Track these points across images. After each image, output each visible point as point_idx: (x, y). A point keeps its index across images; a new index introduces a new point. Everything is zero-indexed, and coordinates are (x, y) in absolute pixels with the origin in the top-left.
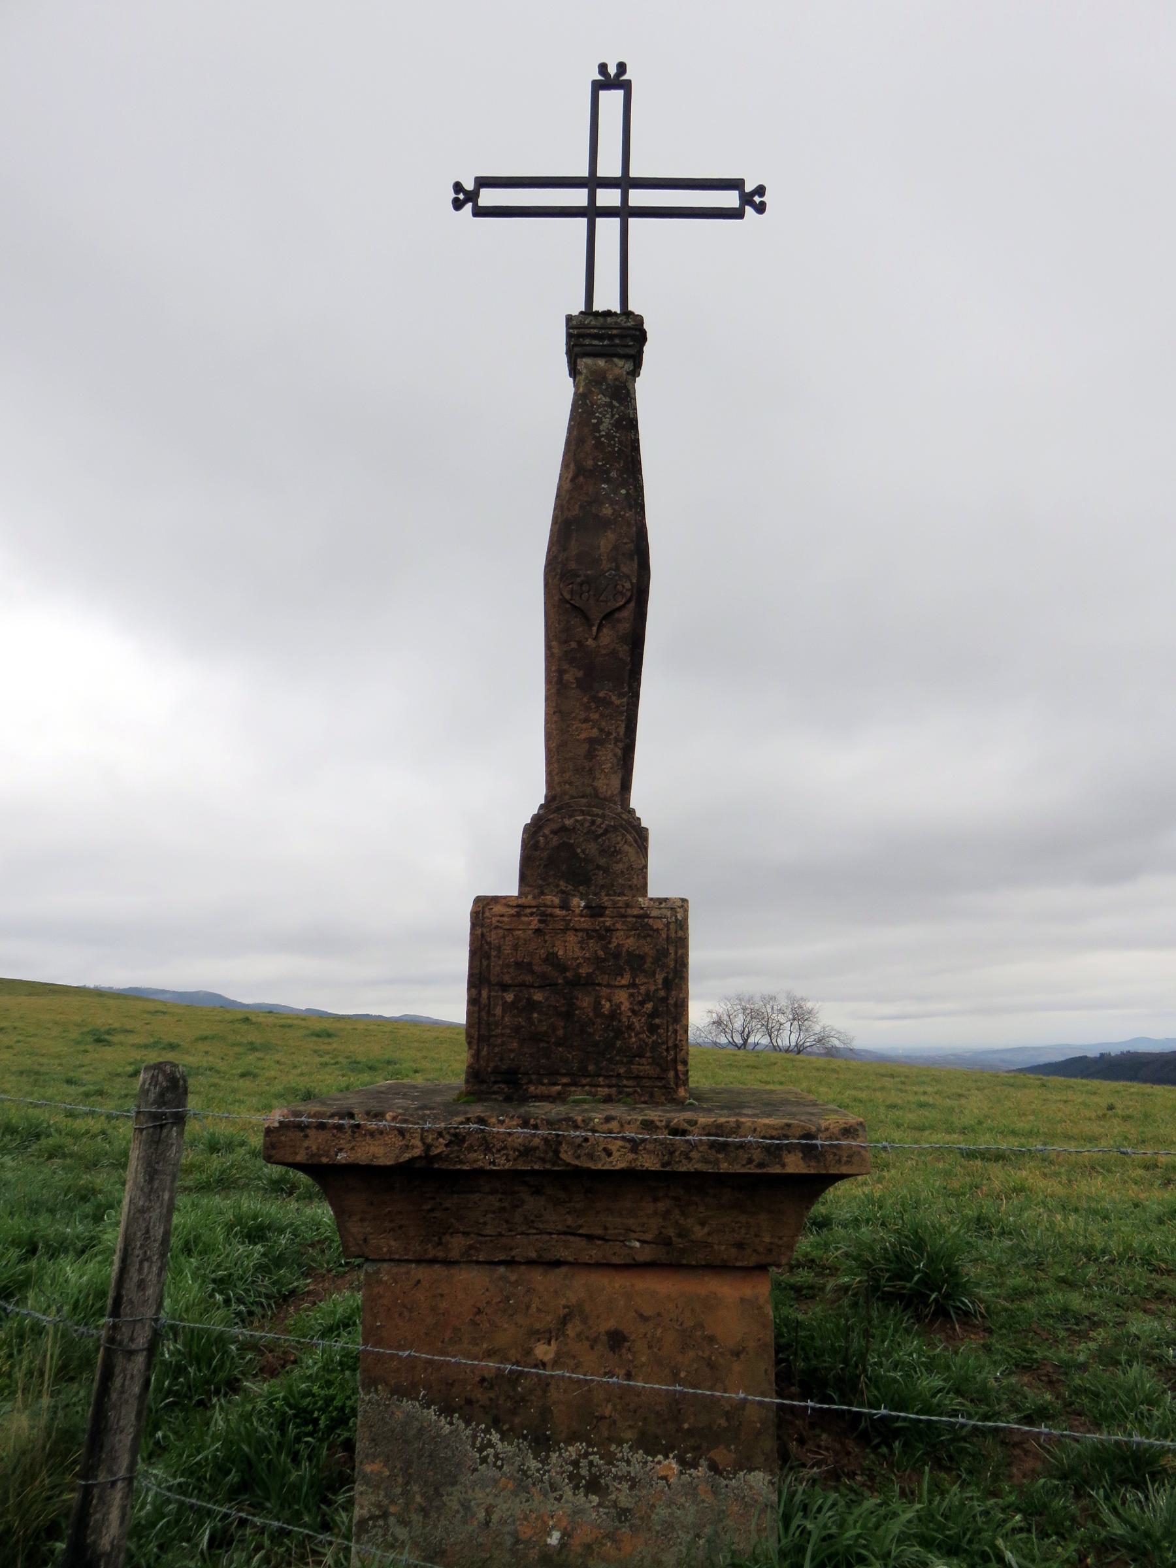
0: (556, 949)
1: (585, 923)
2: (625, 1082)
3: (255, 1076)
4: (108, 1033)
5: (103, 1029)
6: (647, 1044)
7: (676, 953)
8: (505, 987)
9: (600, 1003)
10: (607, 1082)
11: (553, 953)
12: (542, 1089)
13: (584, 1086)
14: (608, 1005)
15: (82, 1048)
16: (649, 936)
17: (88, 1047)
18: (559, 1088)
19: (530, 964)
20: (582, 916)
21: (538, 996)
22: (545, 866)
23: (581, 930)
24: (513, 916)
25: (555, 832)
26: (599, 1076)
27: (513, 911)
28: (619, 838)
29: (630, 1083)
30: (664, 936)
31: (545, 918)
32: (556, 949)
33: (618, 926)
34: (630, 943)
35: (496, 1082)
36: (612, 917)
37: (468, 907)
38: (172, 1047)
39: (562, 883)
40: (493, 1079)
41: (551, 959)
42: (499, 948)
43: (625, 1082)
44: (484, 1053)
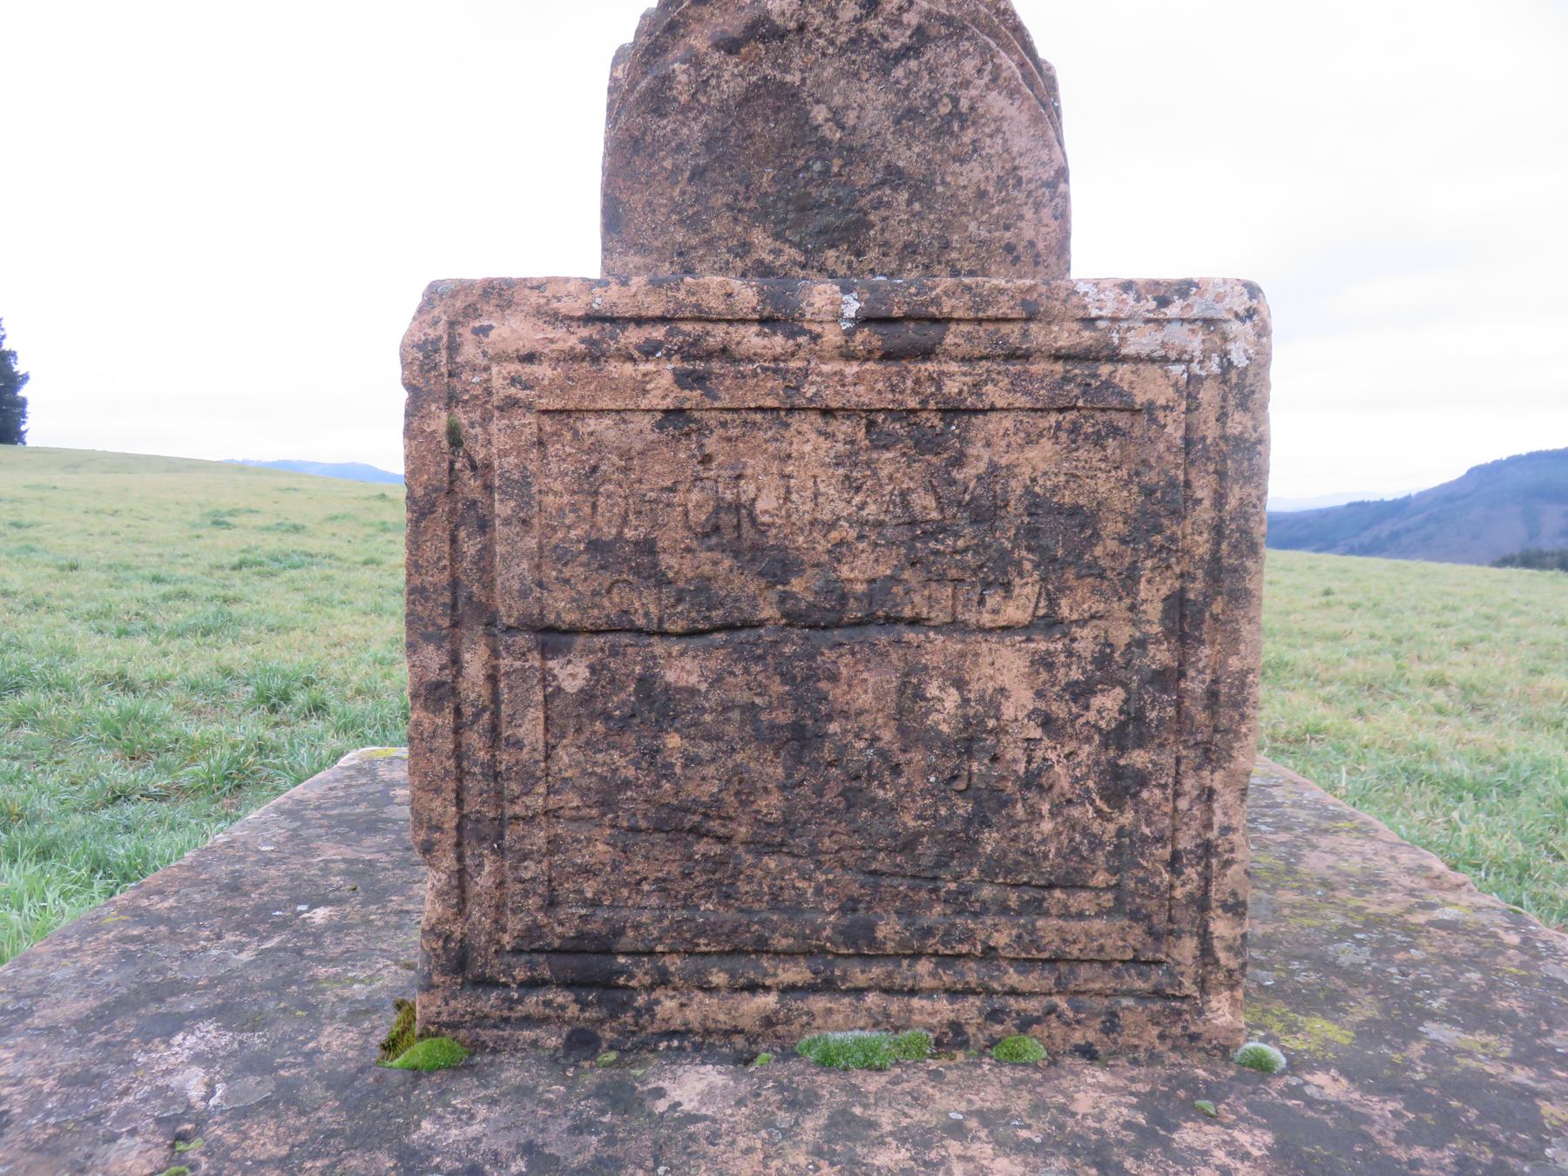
0: (748, 489)
1: (866, 384)
2: (1013, 978)
3: (379, 564)
4: (231, 513)
5: (225, 510)
6: (1096, 843)
7: (1219, 499)
8: (552, 637)
9: (919, 696)
10: (947, 978)
11: (736, 507)
12: (701, 1009)
13: (859, 992)
14: (952, 699)
15: (195, 533)
16: (1115, 431)
17: (203, 532)
18: (770, 1001)
19: (647, 547)
20: (848, 356)
21: (683, 670)
22: (697, 174)
23: (848, 412)
24: (573, 357)
25: (730, 46)
26: (916, 956)
27: (572, 339)
28: (969, 65)
29: (1032, 981)
30: (1175, 433)
31: (700, 364)
32: (748, 489)
33: (995, 394)
34: (1038, 462)
35: (532, 984)
36: (967, 360)
37: (393, 320)
38: (296, 529)
39: (759, 237)
40: (520, 974)
41: (730, 528)
42: (521, 485)
43: (1013, 978)
44: (483, 881)
